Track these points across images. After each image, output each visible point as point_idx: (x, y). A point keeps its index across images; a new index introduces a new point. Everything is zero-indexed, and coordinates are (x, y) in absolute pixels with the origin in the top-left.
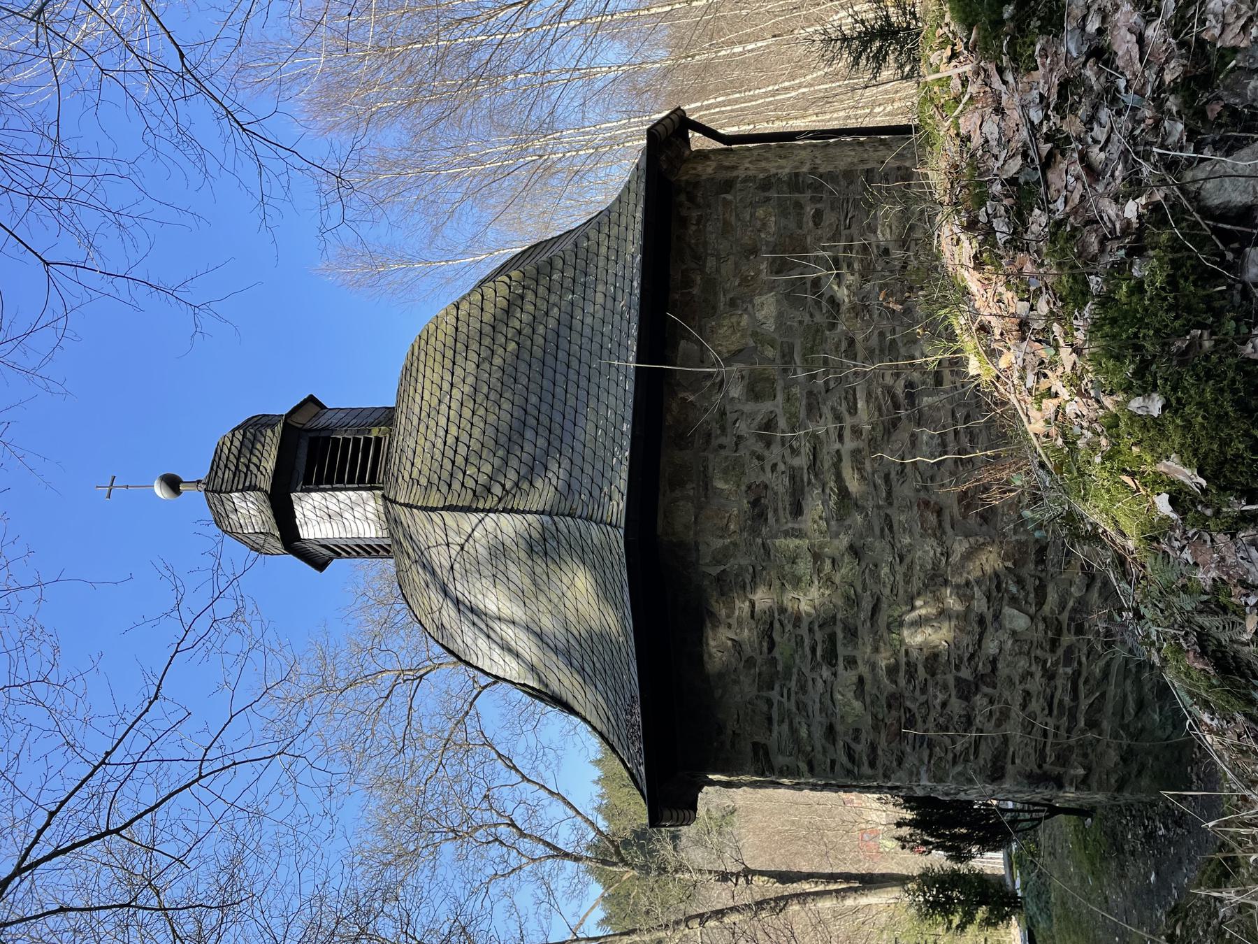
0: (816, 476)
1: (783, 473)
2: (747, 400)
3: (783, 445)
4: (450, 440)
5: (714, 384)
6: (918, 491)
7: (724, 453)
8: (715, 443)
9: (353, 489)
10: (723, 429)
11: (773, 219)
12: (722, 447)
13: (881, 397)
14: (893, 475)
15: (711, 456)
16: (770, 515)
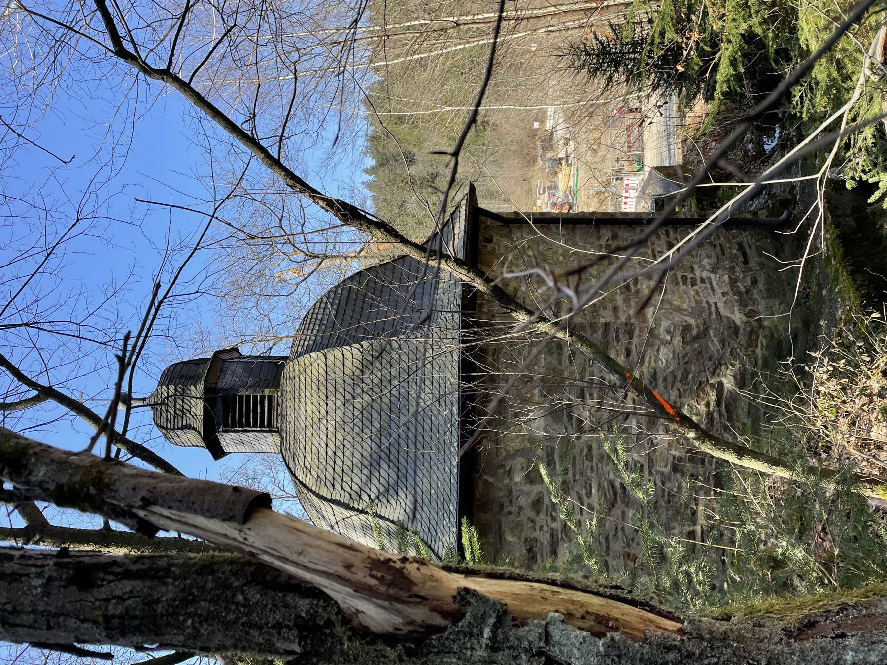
0: (566, 534)
1: (547, 532)
2: (526, 483)
3: (547, 515)
4: (330, 453)
5: (505, 472)
6: (624, 547)
7: (511, 517)
8: (506, 510)
9: (258, 432)
10: (511, 502)
11: (543, 356)
12: (510, 513)
13: (606, 487)
14: (611, 536)
15: (503, 519)
16: (538, 558)
